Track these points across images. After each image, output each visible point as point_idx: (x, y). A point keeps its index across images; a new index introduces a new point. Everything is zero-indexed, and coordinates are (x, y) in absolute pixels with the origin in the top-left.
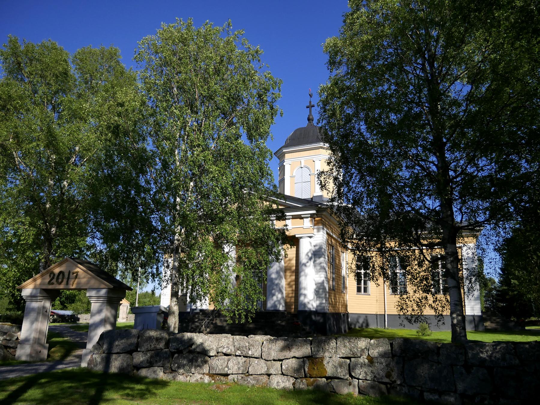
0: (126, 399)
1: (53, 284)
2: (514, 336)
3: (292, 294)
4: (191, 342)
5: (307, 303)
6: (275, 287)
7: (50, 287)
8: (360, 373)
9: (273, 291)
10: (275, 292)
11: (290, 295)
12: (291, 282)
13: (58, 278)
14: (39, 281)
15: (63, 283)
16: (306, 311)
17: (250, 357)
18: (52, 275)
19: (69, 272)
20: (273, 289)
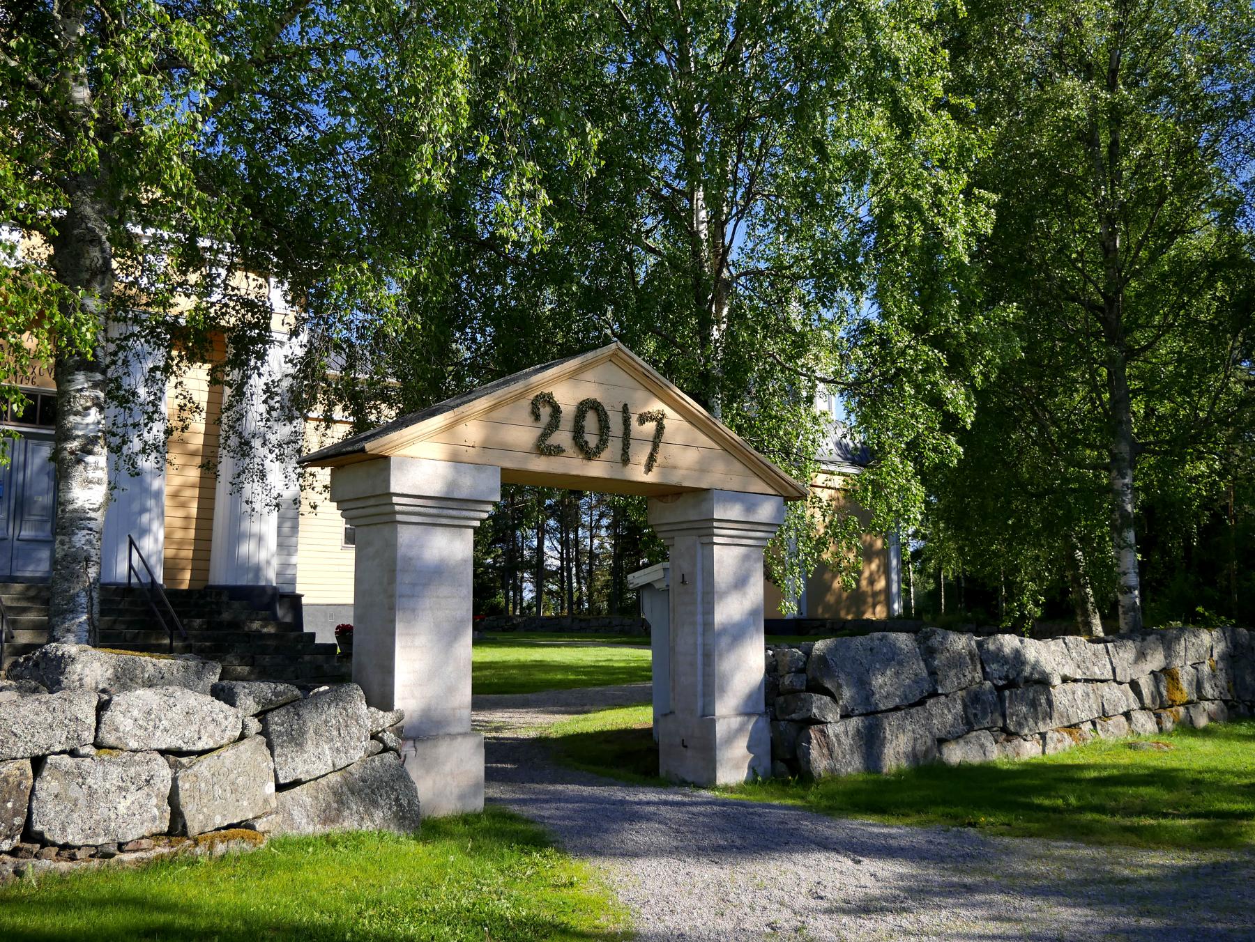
0: (1222, 772)
1: (558, 451)
2: (488, 650)
3: (186, 528)
4: (1018, 658)
5: (263, 563)
6: (151, 503)
7: (541, 465)
8: (1209, 690)
9: (145, 518)
10: (151, 520)
11: (179, 534)
12: (184, 486)
13: (578, 431)
14: (472, 431)
15: (605, 455)
16: (263, 588)
17: (1097, 681)
18: (545, 412)
19: (625, 409)
20: (144, 510)
